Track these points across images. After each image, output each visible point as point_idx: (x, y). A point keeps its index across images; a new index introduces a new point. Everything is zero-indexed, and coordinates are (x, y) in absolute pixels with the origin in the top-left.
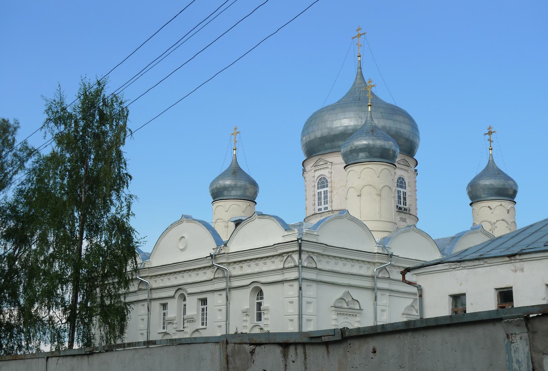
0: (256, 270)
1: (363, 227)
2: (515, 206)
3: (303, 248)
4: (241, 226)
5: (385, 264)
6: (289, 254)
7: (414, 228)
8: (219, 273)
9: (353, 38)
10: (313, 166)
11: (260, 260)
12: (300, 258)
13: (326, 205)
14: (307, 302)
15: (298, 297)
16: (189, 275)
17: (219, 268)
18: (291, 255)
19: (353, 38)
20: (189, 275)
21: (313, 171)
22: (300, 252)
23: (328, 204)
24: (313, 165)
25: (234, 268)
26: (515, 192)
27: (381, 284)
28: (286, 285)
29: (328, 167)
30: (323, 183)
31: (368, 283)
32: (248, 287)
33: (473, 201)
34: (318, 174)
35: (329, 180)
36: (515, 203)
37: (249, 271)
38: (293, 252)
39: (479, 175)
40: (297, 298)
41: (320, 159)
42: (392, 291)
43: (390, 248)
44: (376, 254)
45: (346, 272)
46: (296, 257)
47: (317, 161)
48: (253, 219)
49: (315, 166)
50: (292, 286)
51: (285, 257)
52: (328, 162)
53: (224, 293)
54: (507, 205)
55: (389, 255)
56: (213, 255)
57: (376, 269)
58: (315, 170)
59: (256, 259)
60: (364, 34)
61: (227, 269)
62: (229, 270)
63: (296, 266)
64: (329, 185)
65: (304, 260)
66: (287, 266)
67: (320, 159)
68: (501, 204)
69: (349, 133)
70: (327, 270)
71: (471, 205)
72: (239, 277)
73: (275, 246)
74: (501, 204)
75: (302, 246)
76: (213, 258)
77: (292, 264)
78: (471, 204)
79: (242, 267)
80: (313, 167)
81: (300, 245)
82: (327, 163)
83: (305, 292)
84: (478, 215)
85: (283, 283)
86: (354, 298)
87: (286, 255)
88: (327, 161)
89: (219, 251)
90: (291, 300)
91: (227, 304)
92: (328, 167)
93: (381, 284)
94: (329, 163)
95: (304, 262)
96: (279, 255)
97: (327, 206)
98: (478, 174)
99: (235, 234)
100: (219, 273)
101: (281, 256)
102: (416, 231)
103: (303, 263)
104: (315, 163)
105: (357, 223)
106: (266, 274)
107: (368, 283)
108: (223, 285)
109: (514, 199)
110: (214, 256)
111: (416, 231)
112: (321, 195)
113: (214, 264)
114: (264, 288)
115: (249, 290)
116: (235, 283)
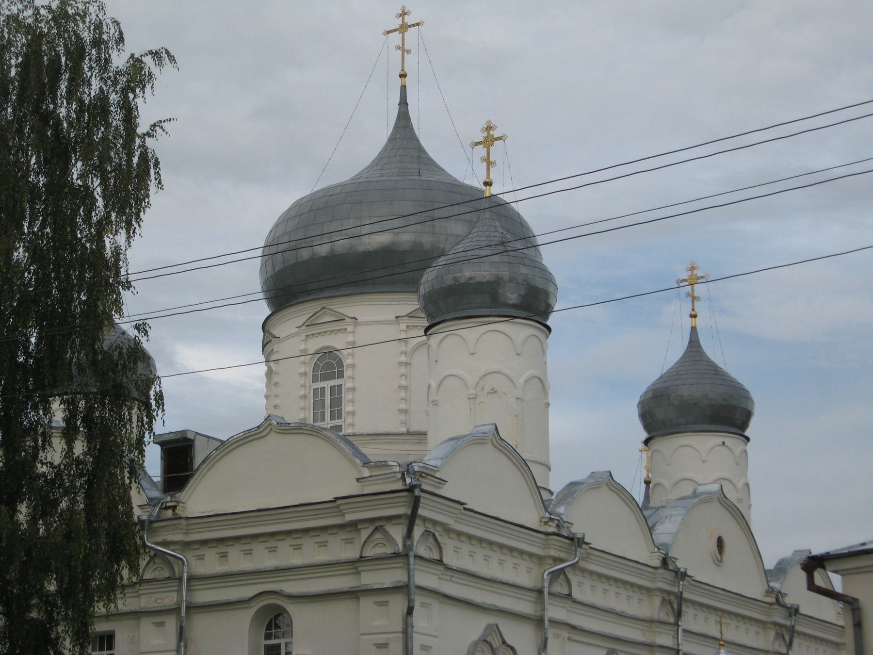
0: (269, 562)
1: (521, 469)
2: (747, 447)
3: (421, 512)
4: (223, 453)
5: (562, 561)
6: (377, 524)
7: (609, 479)
8: (377, 544)
9: (389, 32)
10: (303, 325)
11: (266, 540)
12: (409, 535)
13: (336, 421)
14: (421, 645)
15: (403, 632)
16: (317, 543)
17: (158, 554)
18: (382, 526)
19: (389, 32)
20: (317, 543)
21: (303, 336)
22: (412, 519)
23: (341, 418)
24: (305, 322)
25: (201, 558)
26: (747, 415)
27: (554, 611)
28: (367, 604)
29: (346, 329)
30: (329, 365)
31: (525, 606)
32: (246, 606)
33: (653, 434)
34: (315, 345)
35: (348, 361)
36: (748, 439)
37: (247, 565)
38: (389, 519)
39: (665, 374)
40: (400, 635)
41: (324, 308)
42: (573, 627)
43: (572, 524)
44: (551, 537)
45: (490, 577)
46: (397, 533)
47: (316, 313)
48: (265, 433)
49: (309, 324)
50: (161, 624)
51: (365, 534)
52: (346, 318)
53: (171, 624)
54: (732, 441)
55: (576, 540)
56: (145, 520)
57: (547, 572)
58: (307, 336)
59: (272, 535)
60: (418, 24)
61: (185, 560)
62: (187, 561)
63: (396, 555)
64: (348, 373)
65: (417, 540)
66: (369, 552)
67: (324, 308)
68: (724, 443)
69: (401, 249)
70: (455, 568)
71: (648, 443)
72: (228, 580)
73: (338, 502)
74: (724, 443)
75: (421, 504)
76: (146, 527)
77: (389, 550)
78: (647, 442)
79: (224, 556)
80: (304, 327)
81: (416, 503)
82: (345, 319)
83: (419, 620)
84: (669, 465)
85: (358, 598)
86: (509, 642)
87: (366, 525)
88: (343, 315)
89: (159, 513)
90: (381, 638)
91: (179, 647)
92: (346, 329)
93: (554, 611)
94: (347, 320)
95: (417, 545)
96: (342, 527)
97: (338, 424)
98: (665, 371)
99: (204, 472)
100: (377, 544)
101: (347, 530)
102: (613, 488)
103: (416, 548)
104: (311, 317)
105: (511, 456)
106: (302, 572)
107: (525, 606)
108: (169, 599)
109: (744, 430)
110: (147, 524)
111: (613, 488)
112: (323, 395)
113: (149, 544)
114: (294, 610)
115: (244, 618)
116: (204, 596)
